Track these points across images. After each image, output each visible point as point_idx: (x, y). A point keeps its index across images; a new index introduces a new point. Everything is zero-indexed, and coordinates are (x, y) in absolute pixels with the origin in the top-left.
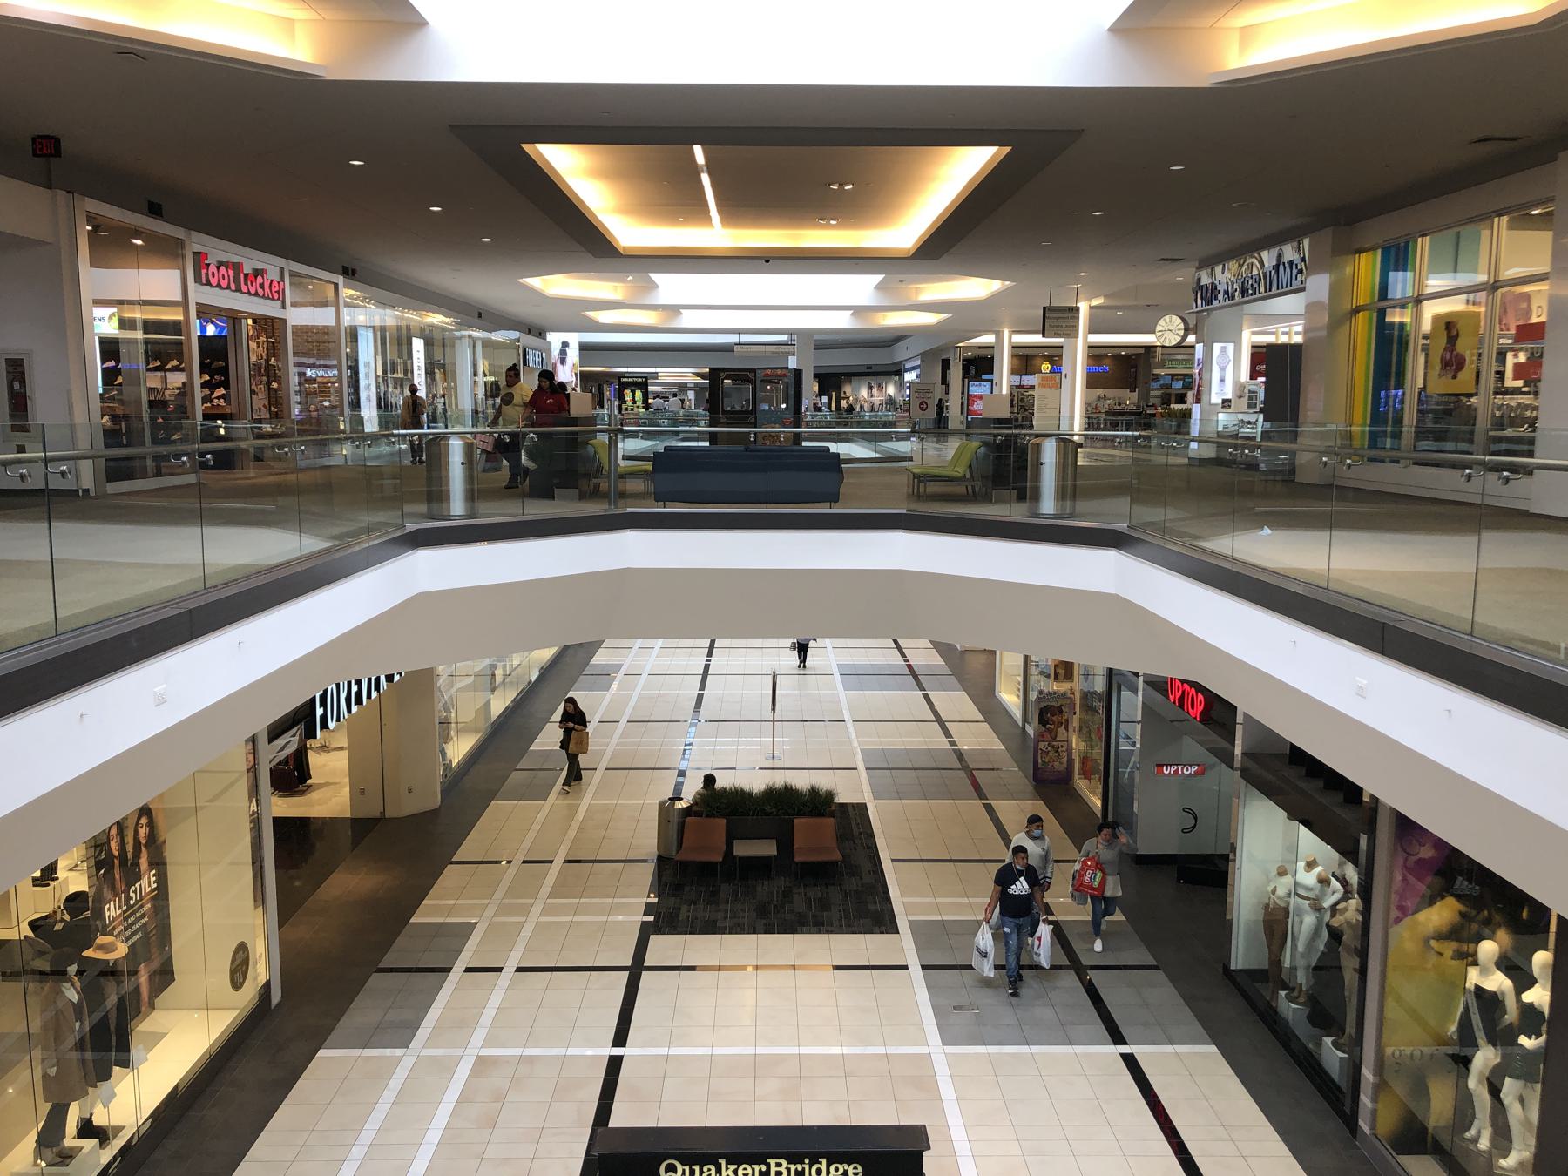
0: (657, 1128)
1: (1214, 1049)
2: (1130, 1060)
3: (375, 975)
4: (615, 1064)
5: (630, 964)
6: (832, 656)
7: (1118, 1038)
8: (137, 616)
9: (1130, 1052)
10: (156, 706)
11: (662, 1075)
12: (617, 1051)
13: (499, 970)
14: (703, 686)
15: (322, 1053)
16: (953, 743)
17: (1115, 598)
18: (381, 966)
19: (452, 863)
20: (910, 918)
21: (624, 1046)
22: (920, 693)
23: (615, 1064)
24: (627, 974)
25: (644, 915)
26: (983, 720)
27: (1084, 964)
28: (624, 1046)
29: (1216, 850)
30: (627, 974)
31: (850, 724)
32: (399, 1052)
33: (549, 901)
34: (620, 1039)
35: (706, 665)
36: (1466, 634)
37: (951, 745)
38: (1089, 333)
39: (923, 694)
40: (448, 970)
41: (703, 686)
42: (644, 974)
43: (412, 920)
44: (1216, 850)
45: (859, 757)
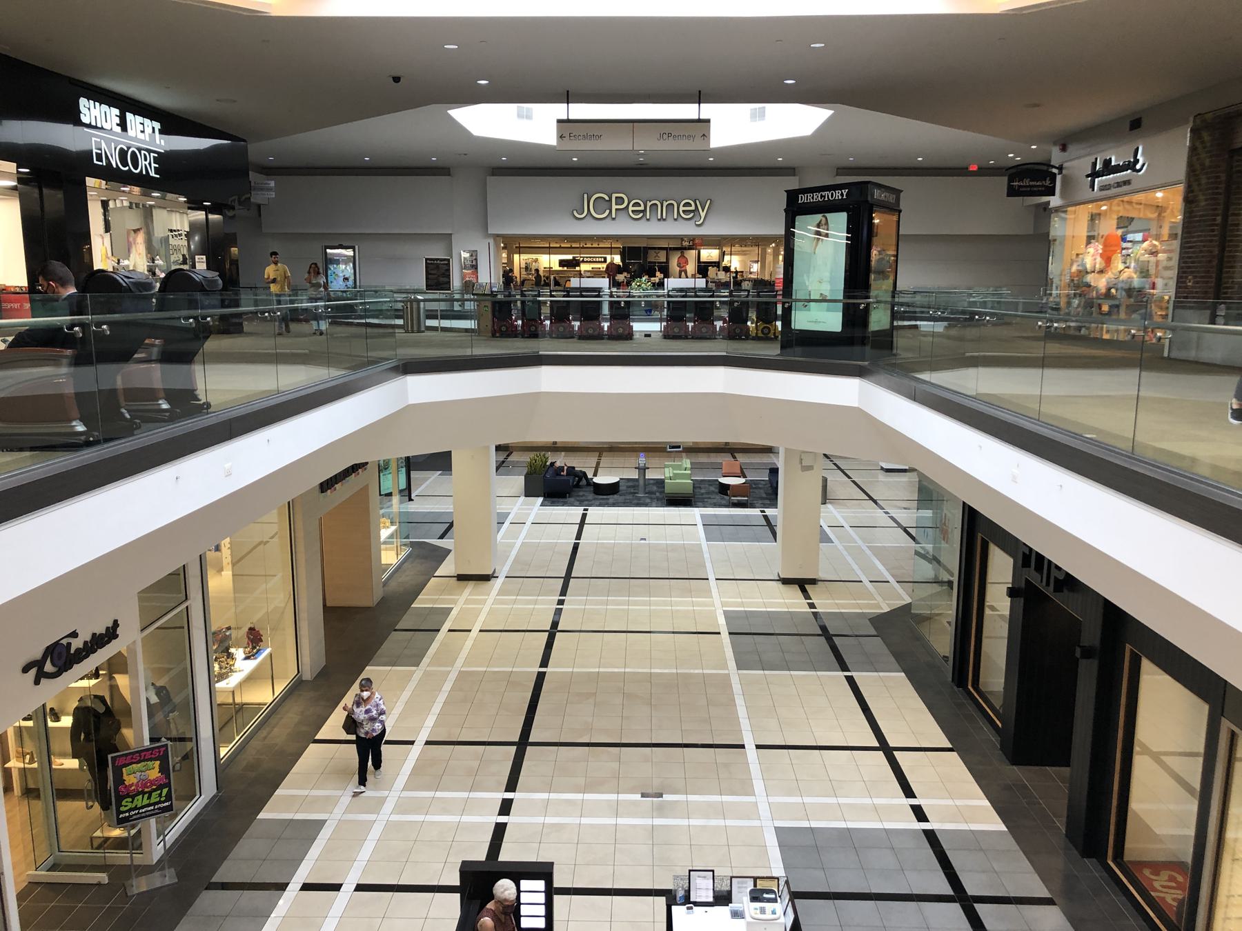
0: (536, 862)
1: (903, 674)
2: (851, 681)
3: (312, 745)
4: (541, 677)
5: (517, 740)
6: (764, 809)
7: (844, 667)
8: (240, 408)
9: (918, 803)
10: (226, 476)
11: (552, 775)
12: (503, 819)
13: (412, 743)
14: (579, 537)
15: (367, 668)
16: (812, 606)
17: (858, 408)
18: (396, 628)
19: (396, 630)
20: (725, 609)
21: (508, 815)
22: (841, 674)
23: (541, 677)
24: (563, 579)
25: (499, 814)
26: (874, 633)
27: (891, 745)
28: (508, 815)
29: (987, 637)
30: (563, 579)
31: (712, 577)
32: (414, 668)
33: (497, 597)
34: (544, 663)
35: (583, 514)
36: (1035, 420)
37: (810, 608)
38: (427, 319)
39: (846, 677)
40: (282, 887)
41: (579, 537)
42: (571, 579)
43: (412, 606)
44: (987, 637)
45: (722, 621)
